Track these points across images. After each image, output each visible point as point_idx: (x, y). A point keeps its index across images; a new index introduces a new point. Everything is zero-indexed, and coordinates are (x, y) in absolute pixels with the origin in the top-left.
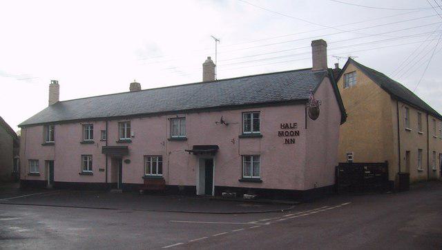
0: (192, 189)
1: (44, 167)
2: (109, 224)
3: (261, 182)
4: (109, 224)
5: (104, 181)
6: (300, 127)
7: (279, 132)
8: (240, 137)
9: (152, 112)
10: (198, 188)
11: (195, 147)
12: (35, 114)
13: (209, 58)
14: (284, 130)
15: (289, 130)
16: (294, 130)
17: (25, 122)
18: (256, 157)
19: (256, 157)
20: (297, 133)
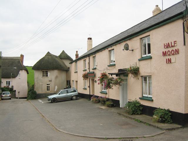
0: (70, 87)
1: (75, 85)
2: (133, 138)
3: (152, 101)
4: (133, 138)
5: (89, 94)
6: (180, 46)
7: (163, 52)
8: (140, 60)
9: (139, 30)
10: (121, 103)
11: (120, 70)
12: (41, 58)
13: (22, 56)
14: (167, 50)
15: (170, 49)
16: (174, 49)
17: (84, 54)
18: (150, 77)
19: (150, 77)
20: (177, 52)
